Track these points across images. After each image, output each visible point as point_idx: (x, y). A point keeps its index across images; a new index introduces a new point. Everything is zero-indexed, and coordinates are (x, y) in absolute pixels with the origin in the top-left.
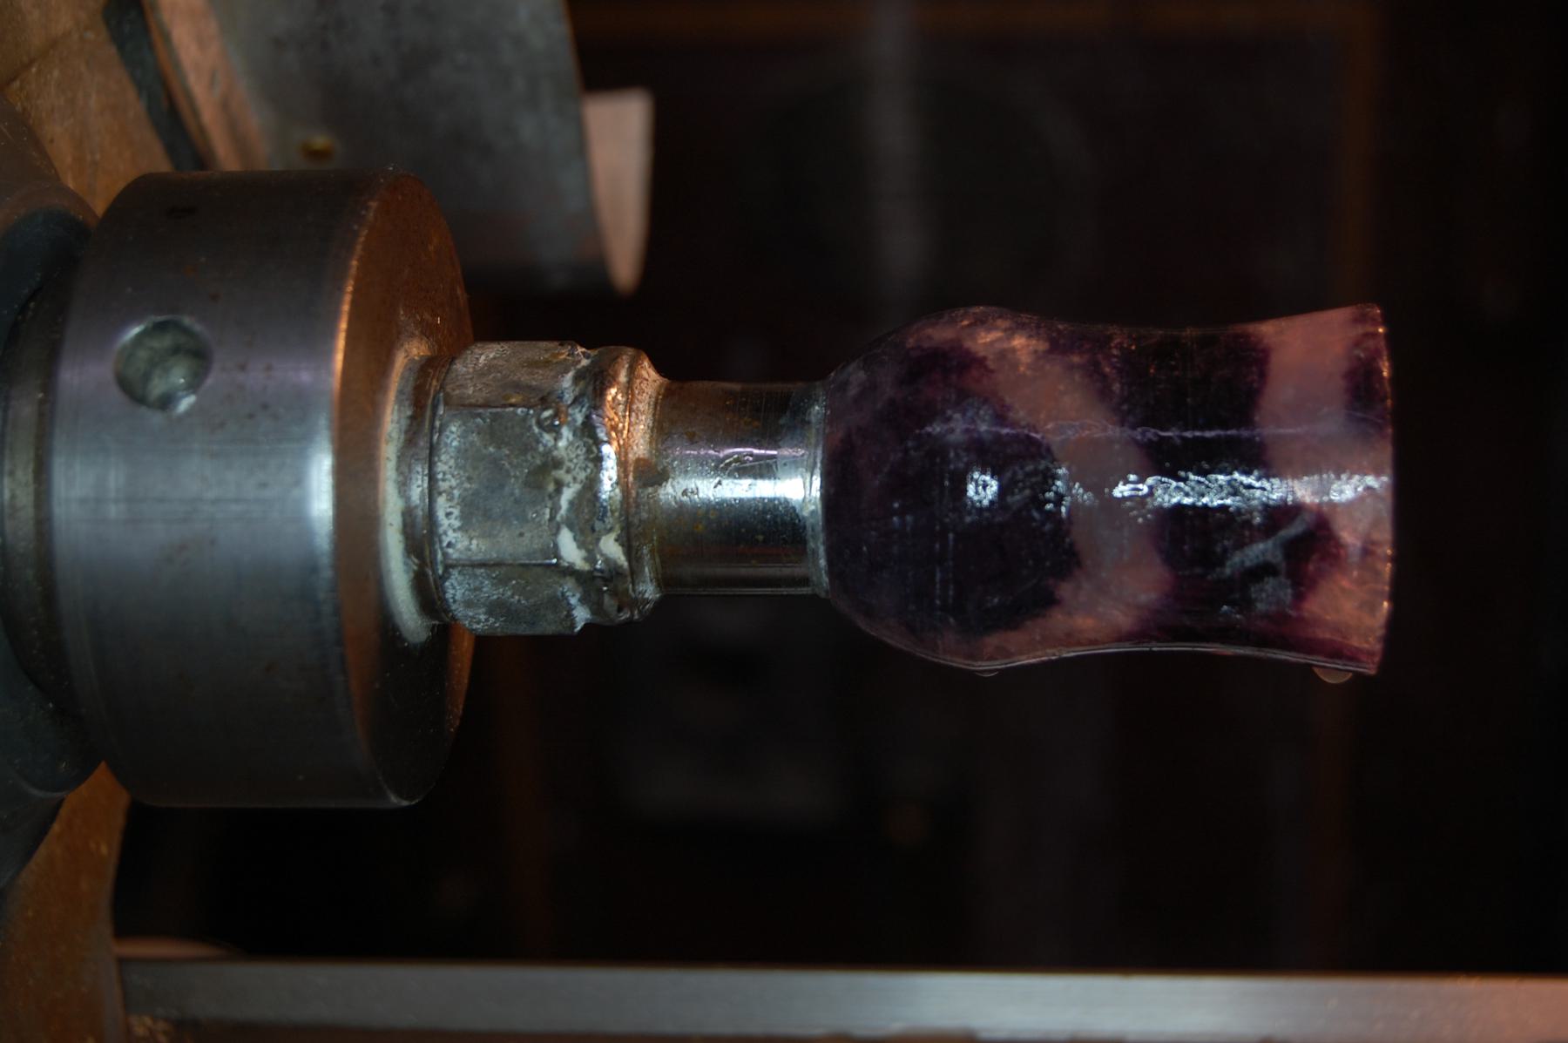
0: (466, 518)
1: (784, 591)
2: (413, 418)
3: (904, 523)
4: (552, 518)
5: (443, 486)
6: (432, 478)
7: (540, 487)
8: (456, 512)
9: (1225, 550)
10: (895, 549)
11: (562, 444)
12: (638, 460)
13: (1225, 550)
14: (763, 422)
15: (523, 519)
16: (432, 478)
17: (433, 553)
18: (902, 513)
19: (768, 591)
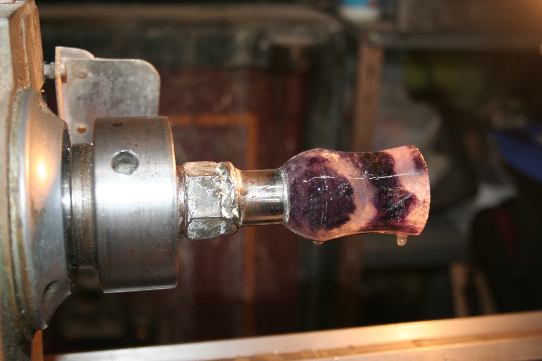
0: (197, 205)
1: (265, 224)
2: (180, 180)
3: (314, 201)
4: (220, 205)
5: (190, 197)
6: (187, 195)
7: (216, 196)
8: (194, 204)
9: (391, 203)
10: (311, 208)
11: (222, 185)
12: (240, 189)
13: (391, 203)
14: (273, 178)
15: (212, 206)
16: (187, 195)
17: (187, 216)
18: (313, 198)
19: (269, 223)
